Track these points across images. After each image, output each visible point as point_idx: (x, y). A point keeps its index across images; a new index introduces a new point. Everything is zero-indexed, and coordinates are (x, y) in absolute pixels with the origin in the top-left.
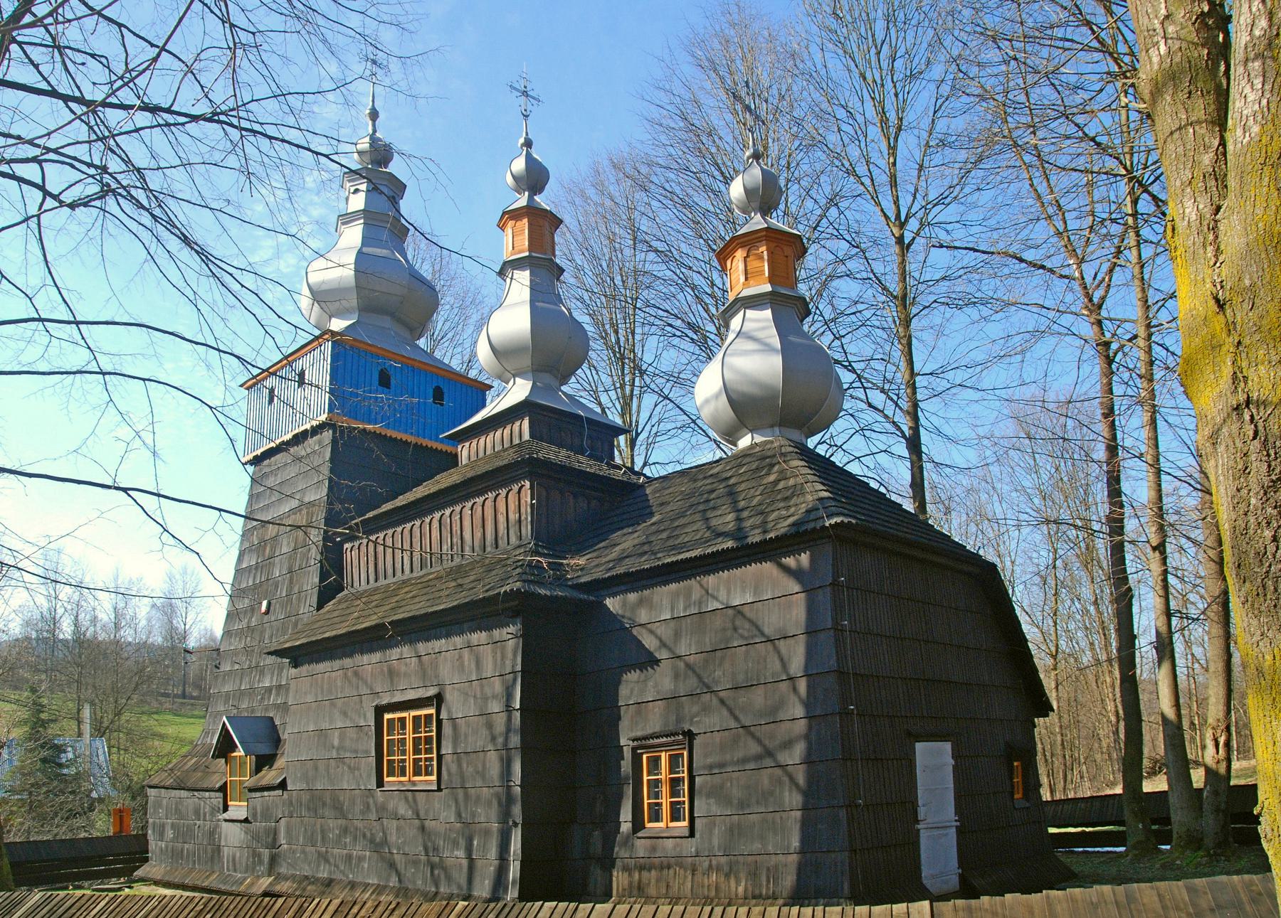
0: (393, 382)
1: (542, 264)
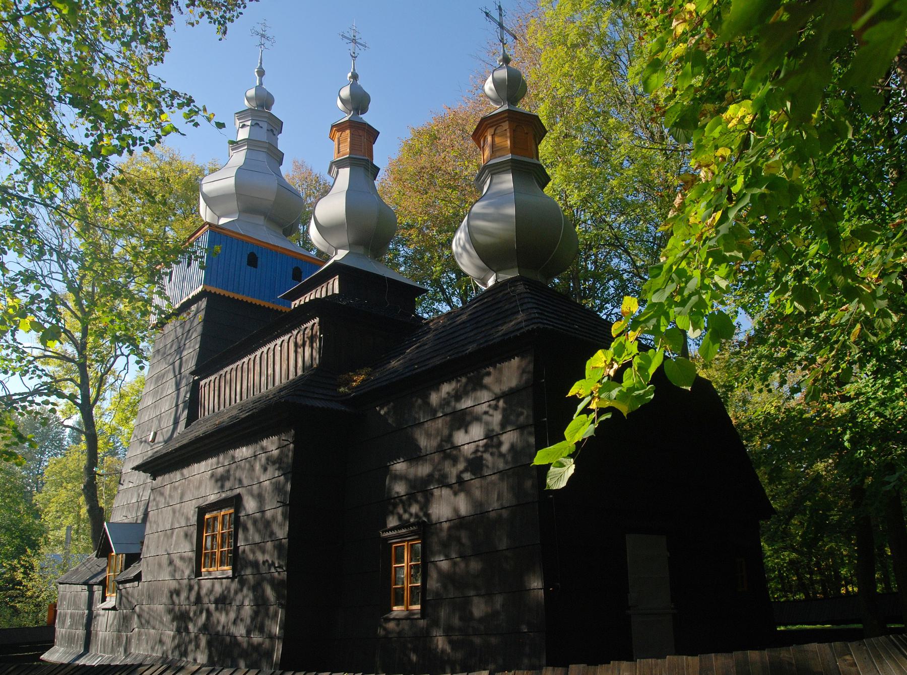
0: (259, 263)
1: (361, 163)
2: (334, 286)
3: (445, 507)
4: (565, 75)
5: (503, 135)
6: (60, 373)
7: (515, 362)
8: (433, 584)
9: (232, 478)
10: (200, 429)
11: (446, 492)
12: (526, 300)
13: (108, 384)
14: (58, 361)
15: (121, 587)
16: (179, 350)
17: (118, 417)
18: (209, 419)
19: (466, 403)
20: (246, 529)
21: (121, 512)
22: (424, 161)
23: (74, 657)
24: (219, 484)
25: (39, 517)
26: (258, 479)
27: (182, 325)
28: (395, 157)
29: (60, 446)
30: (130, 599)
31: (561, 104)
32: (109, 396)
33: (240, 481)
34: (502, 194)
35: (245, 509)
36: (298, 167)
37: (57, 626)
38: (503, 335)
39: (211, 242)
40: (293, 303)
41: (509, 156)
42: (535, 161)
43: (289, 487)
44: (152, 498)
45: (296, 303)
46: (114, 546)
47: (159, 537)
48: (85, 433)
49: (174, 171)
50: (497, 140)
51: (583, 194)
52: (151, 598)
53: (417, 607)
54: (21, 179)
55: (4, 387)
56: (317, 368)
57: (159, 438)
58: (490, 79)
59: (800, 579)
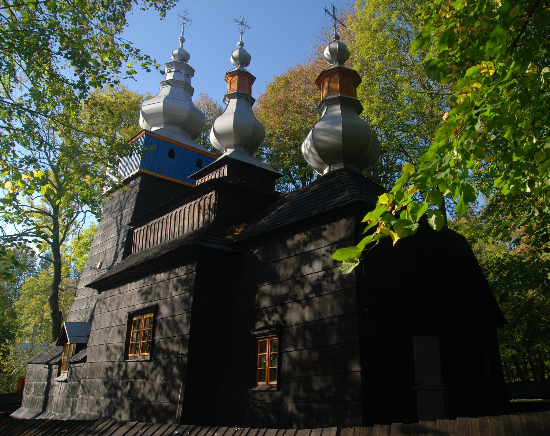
0: (176, 155)
1: (244, 95)
2: (225, 171)
3: (296, 315)
4: (369, 48)
5: (335, 82)
6: (40, 222)
7: (343, 222)
8: (286, 367)
9: (153, 293)
10: (132, 261)
11: (295, 305)
12: (350, 183)
13: (71, 230)
14: (39, 215)
15: (72, 366)
16: (121, 210)
17: (76, 252)
18: (139, 254)
19: (311, 247)
20: (161, 328)
21: (75, 314)
22: (280, 96)
23: (35, 414)
24: (144, 297)
25: (16, 318)
26: (171, 294)
27: (124, 193)
28: (263, 93)
29: (33, 271)
30: (77, 374)
31: (367, 65)
32: (71, 237)
33: (159, 295)
34: (334, 117)
35: (161, 314)
36: (203, 97)
37: (24, 393)
38: (335, 205)
39: (146, 143)
40: (197, 181)
41: (339, 95)
42: (354, 98)
43: (191, 300)
44: (97, 305)
45: (199, 182)
46: (68, 338)
47: (101, 332)
48: (54, 262)
49: (124, 98)
50: (331, 85)
51: (381, 119)
52: (92, 374)
53: (274, 383)
54: (28, 99)
55: (3, 230)
56: (212, 223)
57: (104, 266)
58: (327, 48)
59: (518, 368)
